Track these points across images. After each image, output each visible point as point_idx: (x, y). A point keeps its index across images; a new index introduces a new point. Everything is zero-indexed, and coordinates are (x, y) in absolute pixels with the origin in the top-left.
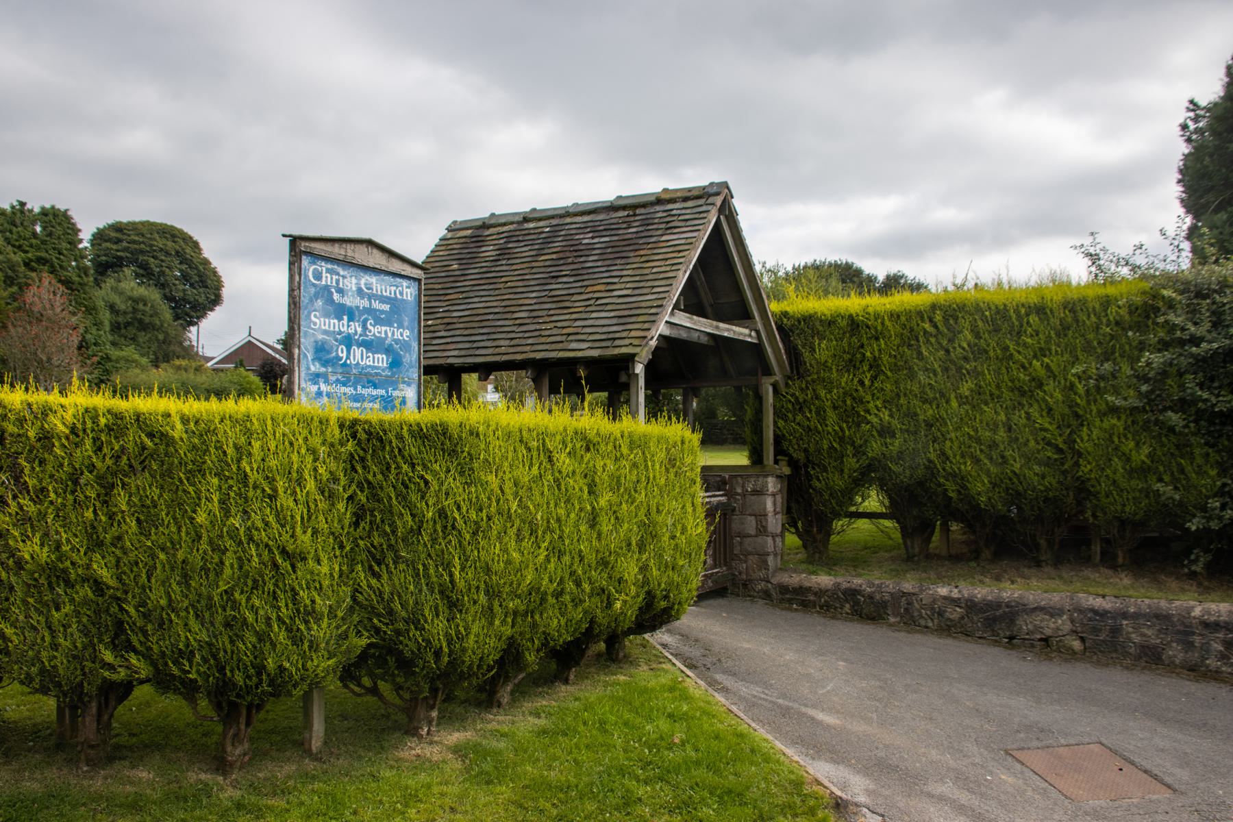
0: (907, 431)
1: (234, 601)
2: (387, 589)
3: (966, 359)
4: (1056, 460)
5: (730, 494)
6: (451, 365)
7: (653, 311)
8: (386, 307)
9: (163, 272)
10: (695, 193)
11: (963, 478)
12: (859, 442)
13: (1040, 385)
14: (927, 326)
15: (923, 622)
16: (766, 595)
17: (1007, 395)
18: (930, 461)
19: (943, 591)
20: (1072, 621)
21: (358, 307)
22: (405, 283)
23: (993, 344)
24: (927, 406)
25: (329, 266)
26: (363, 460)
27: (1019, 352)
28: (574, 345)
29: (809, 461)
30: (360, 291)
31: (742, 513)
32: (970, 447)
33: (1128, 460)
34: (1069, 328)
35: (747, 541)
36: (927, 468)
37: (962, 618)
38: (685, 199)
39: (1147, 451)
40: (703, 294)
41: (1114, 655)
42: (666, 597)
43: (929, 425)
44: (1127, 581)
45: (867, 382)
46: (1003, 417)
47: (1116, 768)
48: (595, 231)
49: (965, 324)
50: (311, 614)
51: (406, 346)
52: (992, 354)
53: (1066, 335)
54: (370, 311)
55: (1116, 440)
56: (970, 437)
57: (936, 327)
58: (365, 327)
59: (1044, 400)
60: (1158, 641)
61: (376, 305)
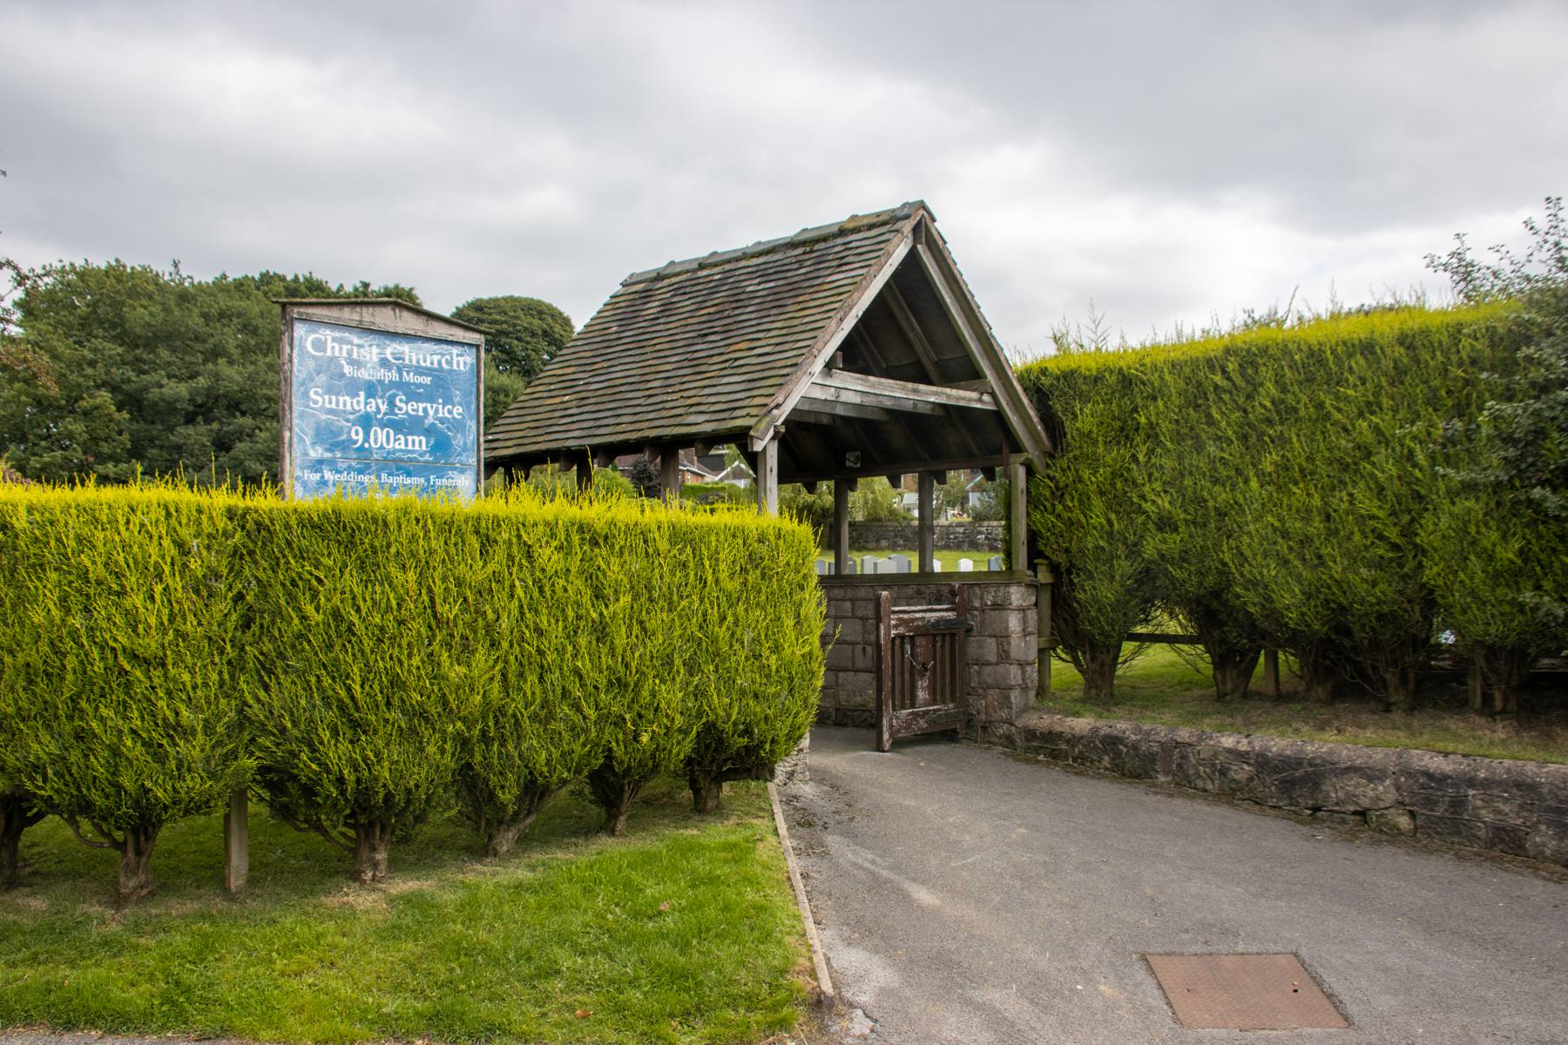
0: (1194, 523)
1: (82, 711)
2: (276, 704)
3: (1269, 422)
4: (1391, 560)
5: (962, 608)
6: (569, 448)
7: (784, 371)
8: (427, 380)
9: (528, 356)
10: (882, 218)
11: (1266, 587)
12: (1132, 539)
13: (1368, 455)
14: (1218, 378)
15: (1200, 784)
16: (1009, 741)
17: (1323, 470)
18: (1225, 564)
19: (1228, 741)
20: (1398, 789)
21: (381, 382)
22: (455, 350)
23: (1305, 399)
24: (1218, 488)
25: (337, 334)
26: (251, 553)
27: (1339, 410)
28: (692, 419)
29: (1072, 565)
30: (384, 363)
31: (981, 634)
32: (1275, 543)
33: (1491, 558)
34: (1406, 373)
35: (987, 670)
36: (1220, 573)
37: (1251, 779)
38: (871, 227)
39: (1517, 546)
40: (919, 350)
41: (1456, 839)
42: (748, 732)
43: (1221, 514)
44: (1501, 735)
45: (1141, 458)
46: (1317, 501)
47: (1290, 989)
48: (763, 274)
49: (1267, 374)
50: (176, 730)
51: (458, 426)
52: (1302, 412)
53: (1402, 383)
54: (401, 385)
55: (1473, 530)
56: (1275, 530)
57: (1229, 379)
58: (392, 404)
59: (1372, 475)
60: (1519, 821)
61: (410, 378)
